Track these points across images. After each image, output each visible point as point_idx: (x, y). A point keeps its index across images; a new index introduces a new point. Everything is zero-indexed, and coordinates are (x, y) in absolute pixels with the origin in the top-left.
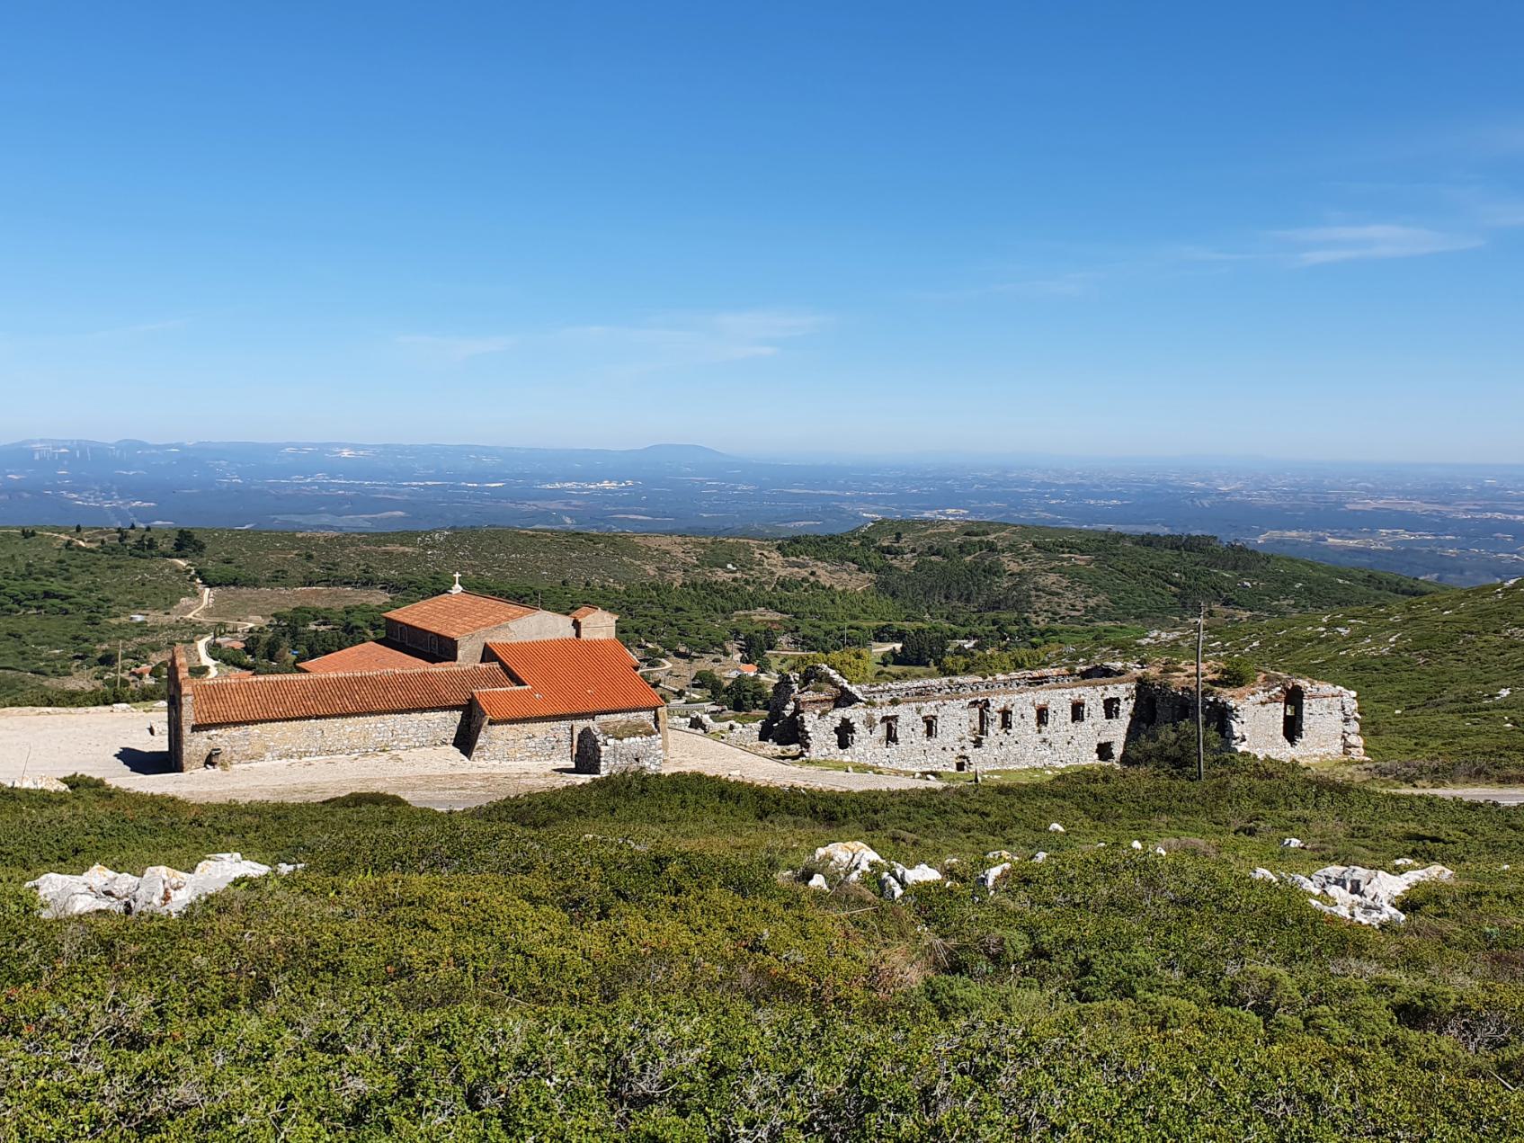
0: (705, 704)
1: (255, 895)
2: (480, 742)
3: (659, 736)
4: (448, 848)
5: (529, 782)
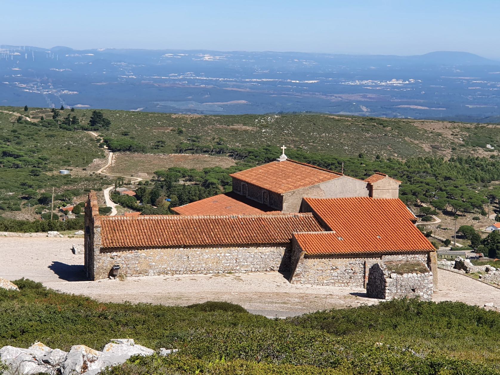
0: (466, 251)
1: (145, 369)
2: (298, 270)
3: (431, 273)
4: (278, 345)
5: (333, 301)
